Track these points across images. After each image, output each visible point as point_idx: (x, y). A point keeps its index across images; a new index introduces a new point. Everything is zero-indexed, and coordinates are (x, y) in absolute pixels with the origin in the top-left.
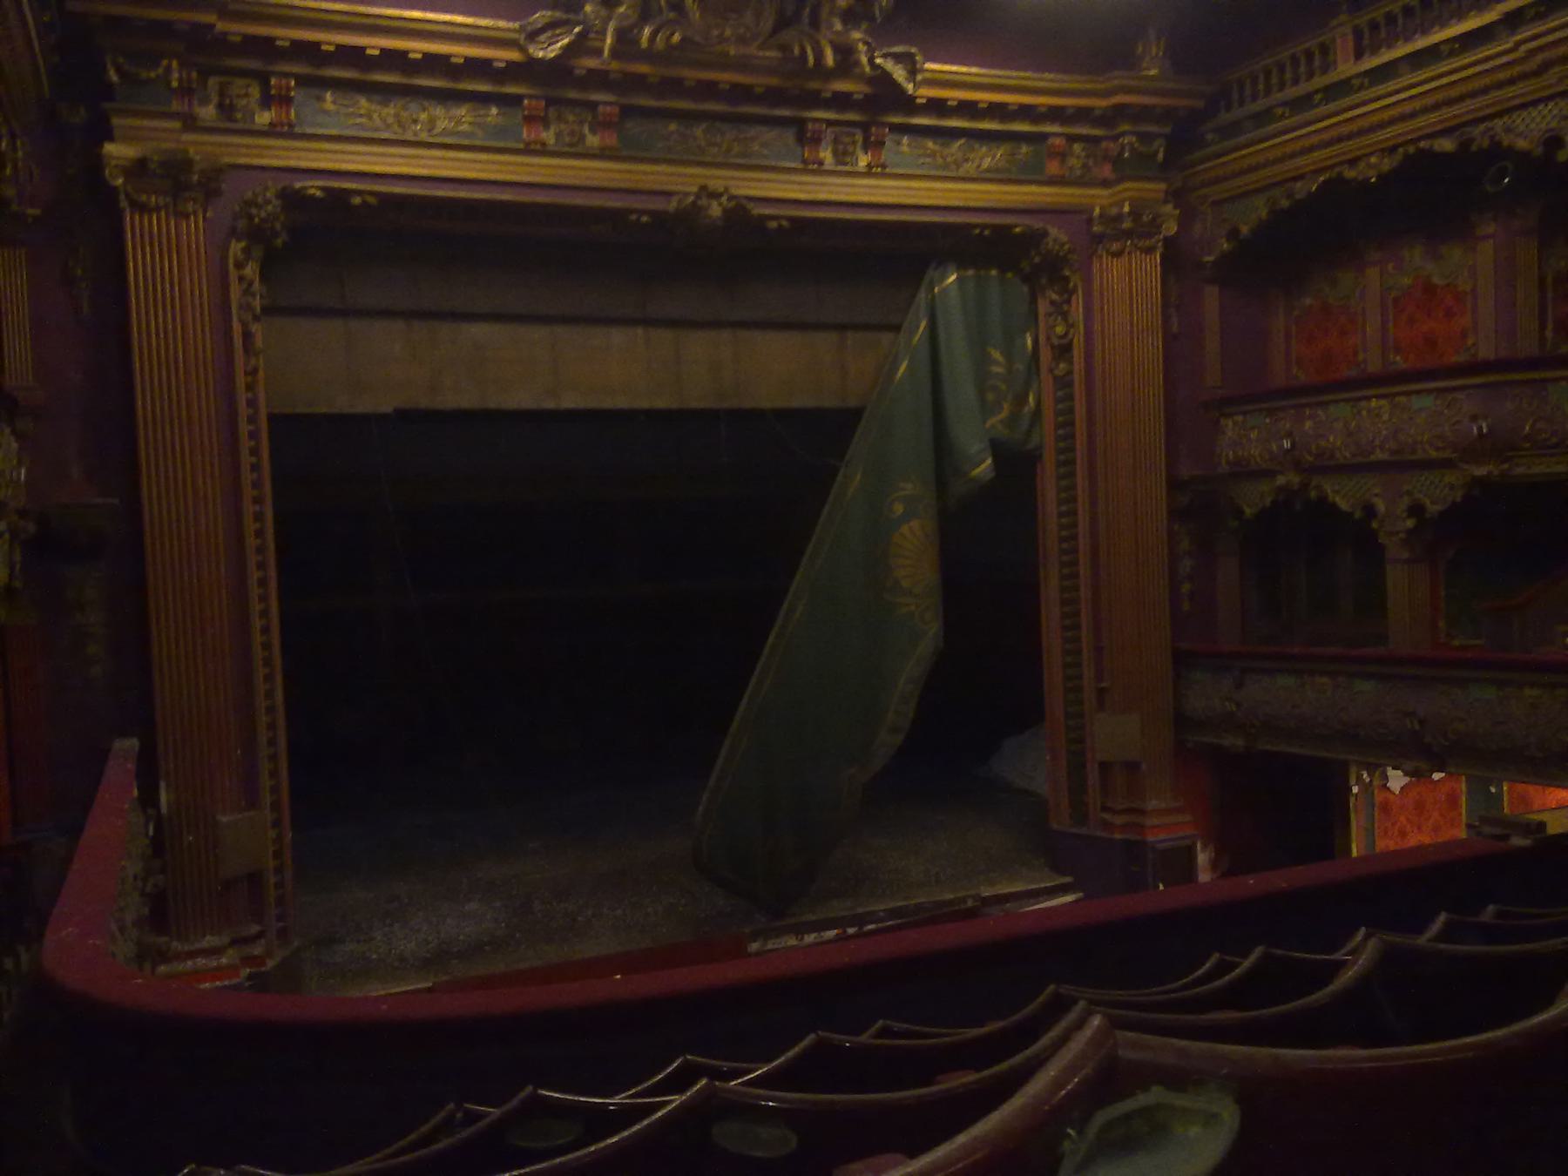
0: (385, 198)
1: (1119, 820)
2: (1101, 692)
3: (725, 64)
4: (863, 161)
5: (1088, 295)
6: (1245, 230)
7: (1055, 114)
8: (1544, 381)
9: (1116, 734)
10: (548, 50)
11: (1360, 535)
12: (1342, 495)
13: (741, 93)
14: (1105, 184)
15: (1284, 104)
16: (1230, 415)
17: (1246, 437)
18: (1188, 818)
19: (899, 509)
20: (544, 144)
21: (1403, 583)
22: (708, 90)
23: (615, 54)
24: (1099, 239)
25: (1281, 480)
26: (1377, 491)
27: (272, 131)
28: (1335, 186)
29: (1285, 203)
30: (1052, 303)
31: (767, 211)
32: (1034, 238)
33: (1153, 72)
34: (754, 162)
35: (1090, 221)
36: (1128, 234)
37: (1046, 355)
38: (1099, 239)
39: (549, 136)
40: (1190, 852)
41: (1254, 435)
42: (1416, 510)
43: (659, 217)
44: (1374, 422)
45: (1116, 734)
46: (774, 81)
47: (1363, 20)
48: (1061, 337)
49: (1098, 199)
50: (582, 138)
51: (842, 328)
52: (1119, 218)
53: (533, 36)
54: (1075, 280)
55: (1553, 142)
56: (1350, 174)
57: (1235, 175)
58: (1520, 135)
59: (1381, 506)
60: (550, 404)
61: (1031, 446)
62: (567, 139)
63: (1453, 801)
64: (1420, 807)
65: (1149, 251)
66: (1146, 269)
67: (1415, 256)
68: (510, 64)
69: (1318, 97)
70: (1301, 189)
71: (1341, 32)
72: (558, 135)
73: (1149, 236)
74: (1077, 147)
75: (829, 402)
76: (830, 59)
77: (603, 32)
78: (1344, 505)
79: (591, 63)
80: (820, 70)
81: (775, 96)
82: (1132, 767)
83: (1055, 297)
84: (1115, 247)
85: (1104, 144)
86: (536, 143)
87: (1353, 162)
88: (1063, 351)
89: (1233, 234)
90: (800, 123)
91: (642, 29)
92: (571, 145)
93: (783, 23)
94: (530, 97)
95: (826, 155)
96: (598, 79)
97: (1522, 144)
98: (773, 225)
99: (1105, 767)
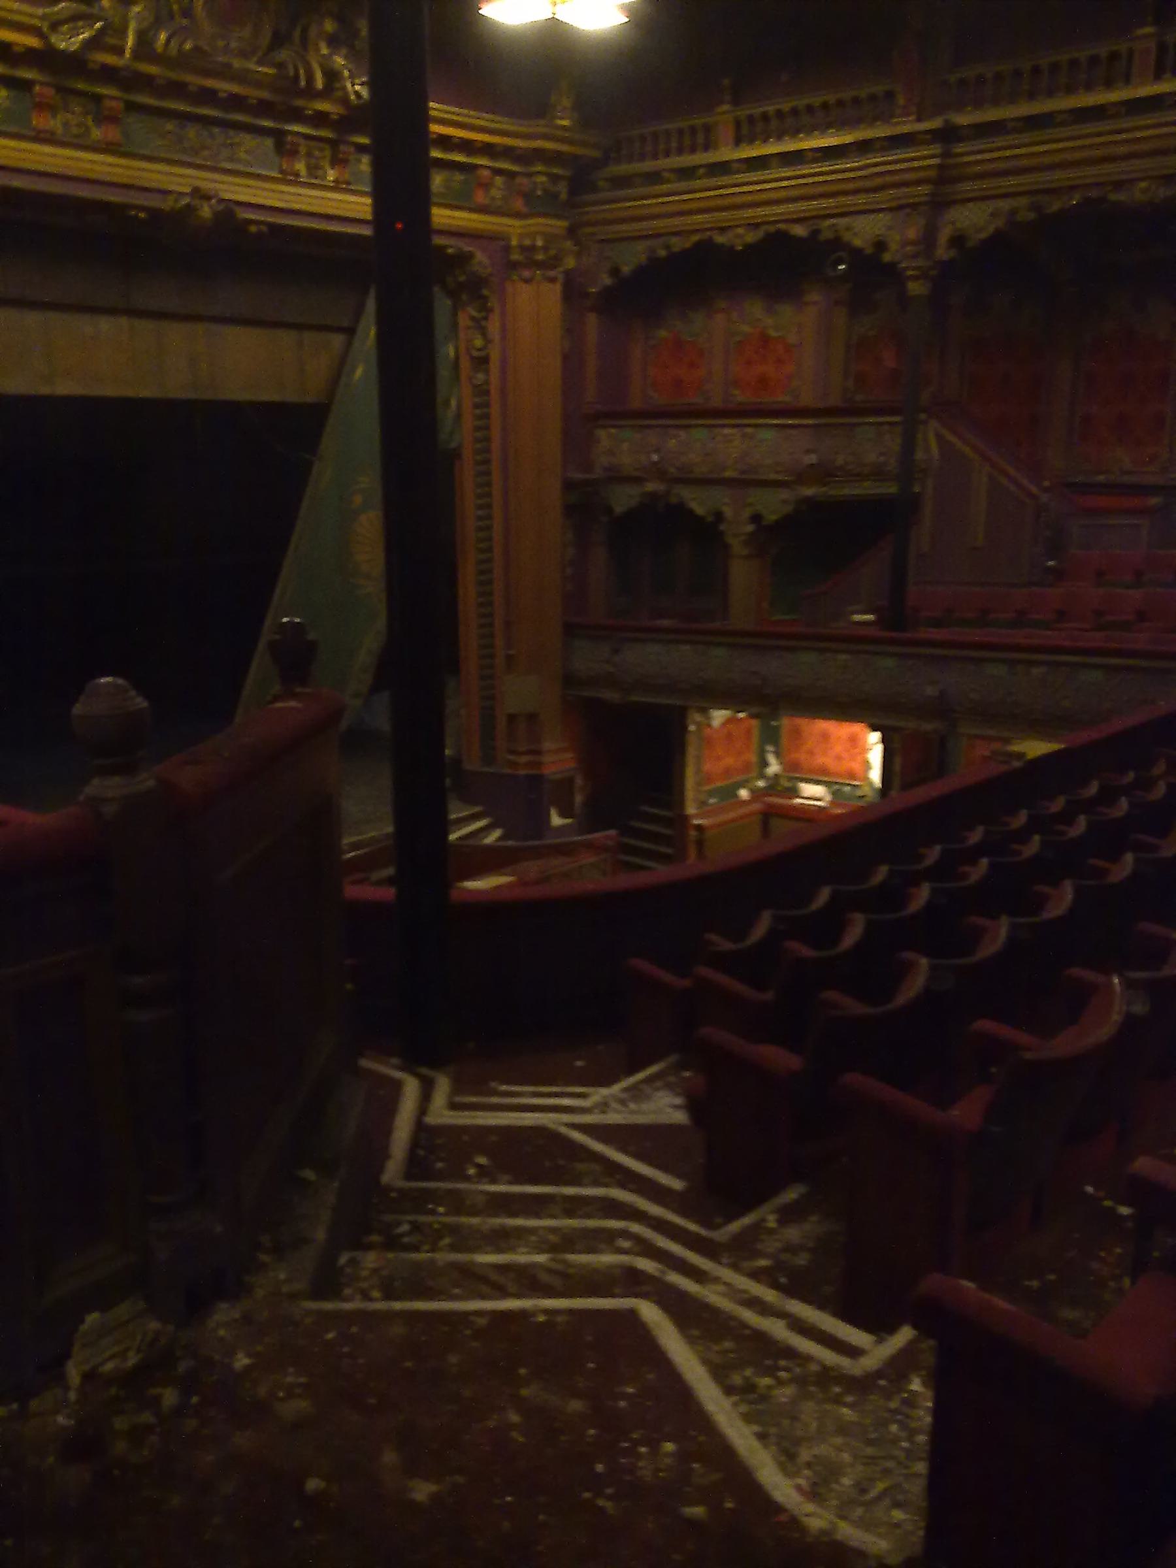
0: (274, 228)
1: (524, 759)
2: (509, 658)
3: (225, 72)
4: (331, 175)
5: (503, 314)
6: (626, 270)
7: (488, 150)
8: (854, 425)
9: (522, 692)
10: (70, 42)
11: (707, 534)
12: (698, 502)
13: (236, 102)
14: (518, 215)
15: (672, 170)
16: (604, 427)
17: (619, 447)
18: (569, 755)
19: (358, 499)
20: (53, 133)
21: (744, 575)
22: (208, 96)
23: (137, 55)
24: (515, 266)
25: (650, 487)
26: (726, 500)
27: (336, 187)
28: (705, 249)
29: (663, 253)
30: (473, 318)
31: (252, 216)
32: (463, 259)
33: (565, 123)
34: (241, 167)
35: (507, 249)
36: (540, 265)
37: (465, 363)
38: (515, 266)
39: (54, 124)
40: (571, 781)
41: (625, 446)
42: (756, 518)
43: (155, 215)
44: (731, 446)
45: (522, 692)
46: (265, 94)
47: (743, 112)
48: (479, 350)
49: (514, 228)
50: (88, 129)
51: (299, 327)
52: (532, 249)
53: (55, 26)
54: (493, 303)
55: (880, 245)
56: (720, 239)
57: (623, 221)
58: (855, 234)
59: (728, 512)
60: (45, 390)
61: (453, 445)
62: (75, 130)
63: (748, 732)
64: (729, 737)
65: (552, 280)
66: (552, 295)
67: (755, 308)
68: (30, 50)
69: (701, 171)
70: (678, 244)
71: (724, 115)
72: (66, 125)
73: (554, 267)
74: (499, 180)
75: (290, 396)
76: (319, 83)
77: (123, 32)
78: (700, 510)
79: (110, 59)
80: (310, 92)
81: (264, 108)
82: (532, 717)
83: (474, 313)
84: (526, 274)
85: (519, 180)
86: (46, 131)
87: (723, 230)
88: (482, 362)
89: (615, 272)
90: (279, 136)
91: (156, 35)
92: (77, 136)
93: (279, 40)
94: (42, 84)
95: (301, 167)
96: (108, 74)
97: (857, 242)
98: (253, 229)
99: (512, 718)
